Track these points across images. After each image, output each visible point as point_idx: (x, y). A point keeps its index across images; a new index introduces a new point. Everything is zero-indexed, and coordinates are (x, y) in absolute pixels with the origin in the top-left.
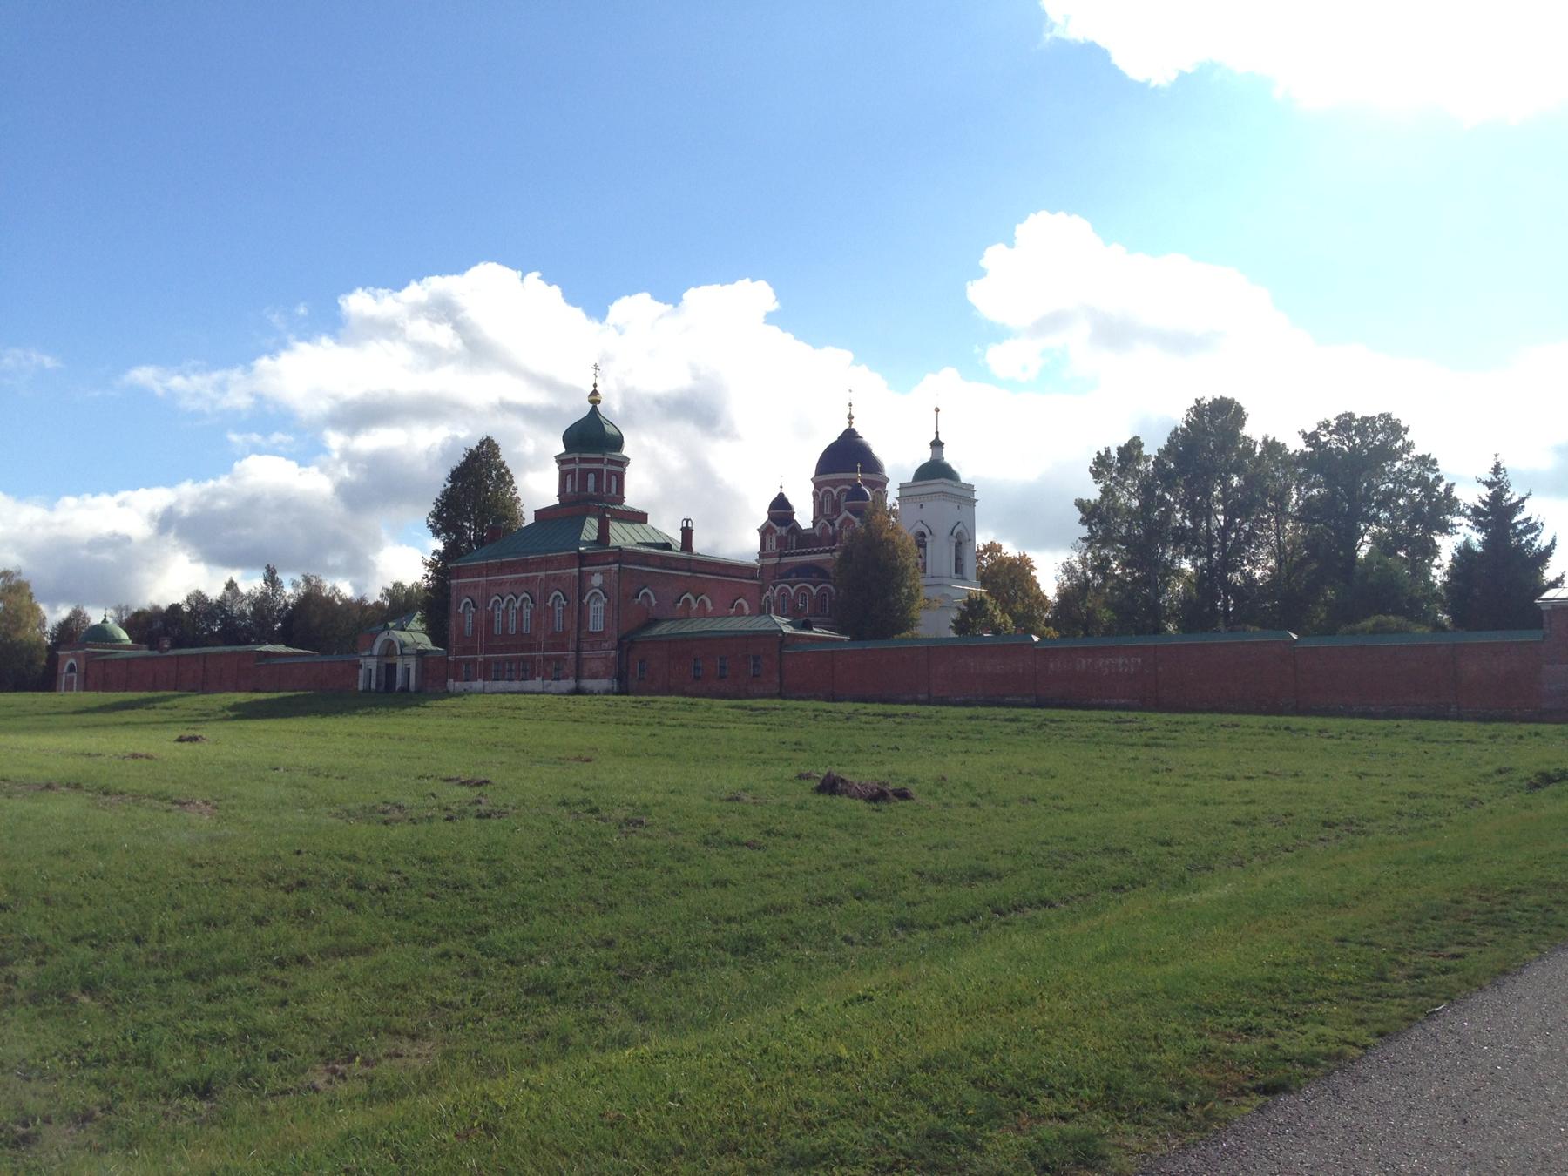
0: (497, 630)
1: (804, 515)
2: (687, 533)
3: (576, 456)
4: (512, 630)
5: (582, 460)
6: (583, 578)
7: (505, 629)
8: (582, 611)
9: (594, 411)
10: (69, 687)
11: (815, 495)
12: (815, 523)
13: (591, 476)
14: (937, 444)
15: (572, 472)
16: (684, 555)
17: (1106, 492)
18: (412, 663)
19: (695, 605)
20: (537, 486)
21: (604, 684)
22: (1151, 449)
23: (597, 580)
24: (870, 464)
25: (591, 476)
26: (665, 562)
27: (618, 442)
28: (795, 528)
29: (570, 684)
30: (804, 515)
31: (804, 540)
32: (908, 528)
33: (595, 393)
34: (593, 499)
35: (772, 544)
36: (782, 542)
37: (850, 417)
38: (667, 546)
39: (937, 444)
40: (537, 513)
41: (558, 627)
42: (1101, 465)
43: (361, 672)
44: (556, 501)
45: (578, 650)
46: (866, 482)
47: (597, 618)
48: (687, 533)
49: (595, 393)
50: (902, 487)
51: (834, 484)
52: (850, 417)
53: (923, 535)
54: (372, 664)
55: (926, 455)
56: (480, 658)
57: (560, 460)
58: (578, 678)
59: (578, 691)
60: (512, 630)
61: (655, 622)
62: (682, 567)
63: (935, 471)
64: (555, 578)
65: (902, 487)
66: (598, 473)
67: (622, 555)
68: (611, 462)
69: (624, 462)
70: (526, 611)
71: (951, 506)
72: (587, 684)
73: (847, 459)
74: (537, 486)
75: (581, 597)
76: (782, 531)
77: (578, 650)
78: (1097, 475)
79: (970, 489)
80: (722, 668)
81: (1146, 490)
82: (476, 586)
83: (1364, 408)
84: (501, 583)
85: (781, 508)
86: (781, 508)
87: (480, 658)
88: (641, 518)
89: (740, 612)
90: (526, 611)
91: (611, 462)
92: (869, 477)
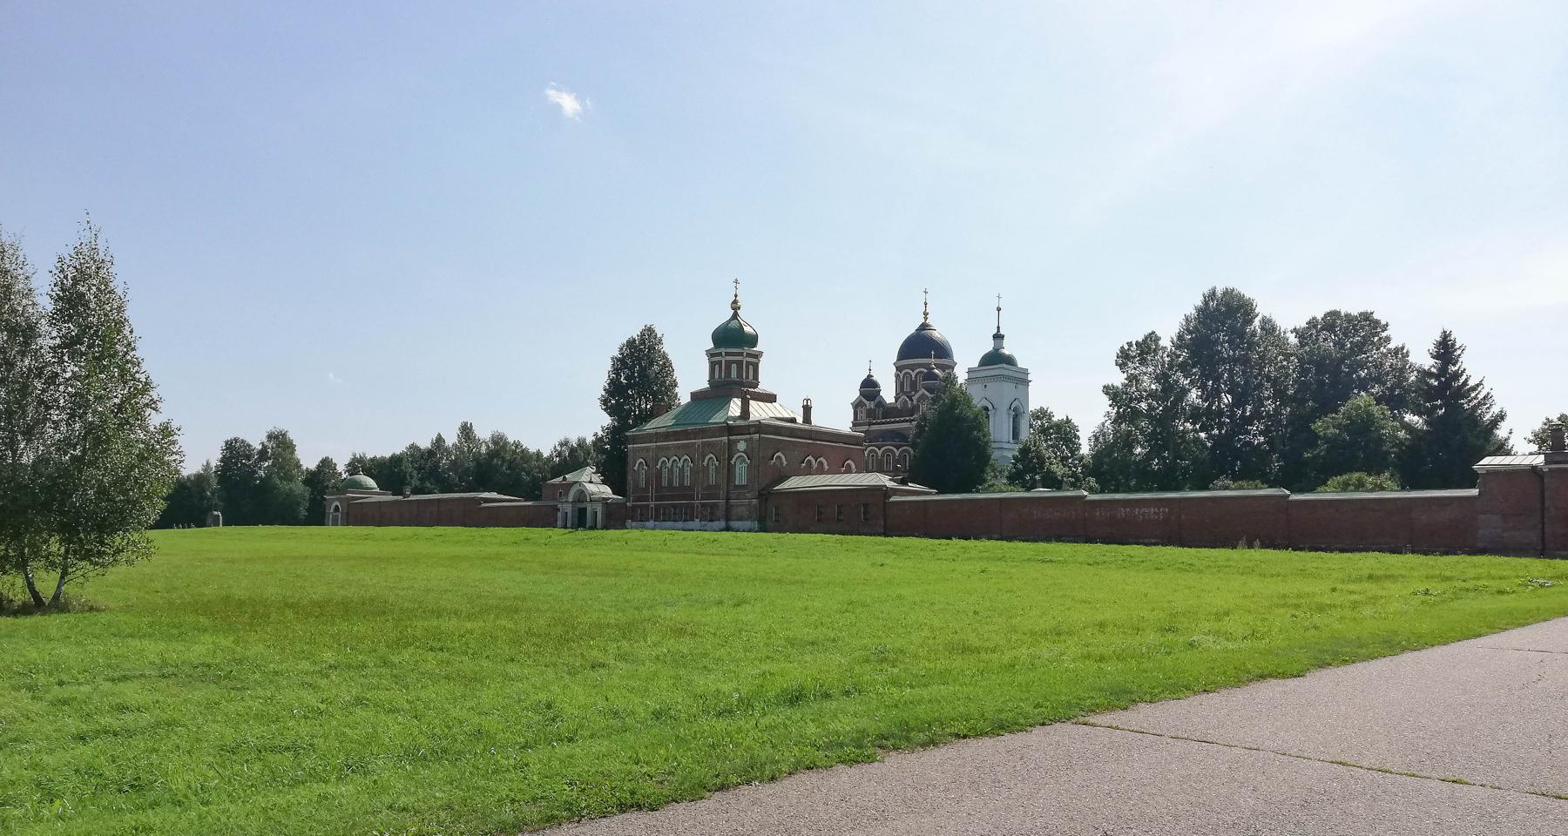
0: (665, 483)
1: (888, 394)
2: (807, 410)
3: (723, 350)
4: (676, 483)
5: (727, 354)
6: (731, 444)
7: (670, 482)
8: (730, 469)
9: (735, 316)
10: (335, 523)
11: (897, 376)
12: (896, 399)
13: (734, 366)
14: (998, 337)
15: (720, 363)
16: (806, 427)
17: (1132, 379)
18: (599, 508)
19: (815, 465)
20: (691, 374)
21: (748, 524)
22: (1166, 342)
23: (742, 446)
24: (942, 350)
25: (734, 366)
26: (793, 432)
27: (753, 340)
28: (881, 403)
29: (723, 524)
30: (888, 394)
31: (889, 412)
32: (978, 398)
33: (735, 302)
34: (735, 383)
35: (862, 415)
36: (870, 413)
37: (926, 314)
38: (793, 420)
39: (998, 337)
40: (693, 395)
41: (712, 481)
42: (1124, 358)
43: (559, 515)
44: (707, 386)
45: (728, 499)
46: (938, 366)
47: (741, 475)
48: (807, 410)
49: (735, 302)
50: (970, 371)
51: (913, 367)
52: (926, 314)
53: (986, 409)
54: (568, 508)
55: (989, 346)
56: (652, 504)
57: (710, 354)
58: (728, 519)
59: (728, 529)
60: (676, 483)
61: (785, 478)
62: (804, 442)
63: (996, 359)
64: (709, 444)
65: (970, 371)
66: (740, 364)
67: (760, 427)
68: (749, 355)
69: (758, 356)
70: (687, 469)
71: (1008, 387)
72: (734, 524)
73: (922, 348)
74: (691, 374)
75: (730, 458)
76: (870, 405)
77: (728, 499)
78: (1122, 366)
79: (1025, 372)
80: (840, 513)
81: (1162, 378)
82: (647, 449)
83: (1352, 306)
84: (667, 448)
85: (869, 387)
86: (869, 387)
87: (652, 504)
88: (770, 398)
89: (849, 471)
90: (687, 469)
91: (749, 355)
92: (939, 361)
